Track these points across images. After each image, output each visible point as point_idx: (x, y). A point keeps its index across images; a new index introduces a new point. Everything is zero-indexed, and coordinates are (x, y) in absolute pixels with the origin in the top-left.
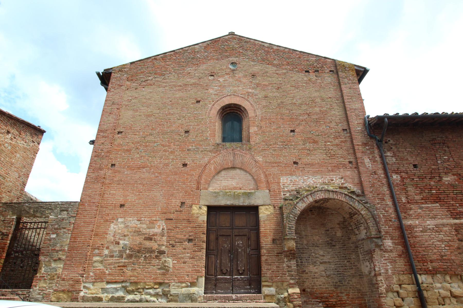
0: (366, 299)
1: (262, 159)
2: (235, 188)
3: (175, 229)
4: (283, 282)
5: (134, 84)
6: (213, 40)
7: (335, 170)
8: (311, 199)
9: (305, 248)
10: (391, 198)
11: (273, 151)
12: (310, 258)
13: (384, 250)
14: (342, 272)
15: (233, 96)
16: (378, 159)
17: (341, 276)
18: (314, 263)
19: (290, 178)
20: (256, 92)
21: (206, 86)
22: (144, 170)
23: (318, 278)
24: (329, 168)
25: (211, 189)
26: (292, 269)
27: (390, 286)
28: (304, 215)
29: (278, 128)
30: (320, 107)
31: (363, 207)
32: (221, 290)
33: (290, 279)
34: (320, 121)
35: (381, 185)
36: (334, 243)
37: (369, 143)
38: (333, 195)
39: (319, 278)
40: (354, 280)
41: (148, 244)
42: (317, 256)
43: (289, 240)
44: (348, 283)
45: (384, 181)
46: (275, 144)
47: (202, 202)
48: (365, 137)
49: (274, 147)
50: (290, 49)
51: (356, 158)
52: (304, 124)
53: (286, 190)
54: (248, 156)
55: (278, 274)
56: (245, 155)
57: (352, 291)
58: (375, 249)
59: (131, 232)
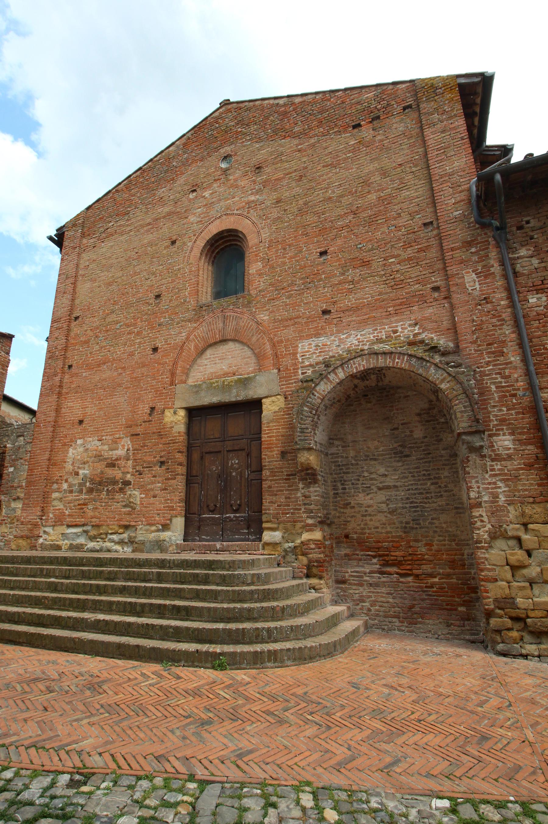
0: (466, 552)
1: (267, 317)
2: (226, 374)
3: (142, 449)
4: (295, 522)
5: (92, 241)
6: (195, 127)
7: (403, 310)
8: (341, 375)
9: (352, 464)
10: (520, 348)
11: (286, 298)
12: (359, 480)
13: (493, 456)
14: (421, 502)
15: (224, 217)
16: (496, 268)
17: (418, 511)
18: (367, 490)
19: (314, 342)
20: (264, 197)
21: (185, 211)
22: (105, 367)
23: (373, 516)
24: (389, 309)
25: (190, 382)
26: (311, 501)
27: (501, 526)
28: (352, 405)
29: (297, 254)
30: (379, 190)
31: (445, 374)
32: (207, 536)
33: (308, 517)
34: (378, 218)
35: (498, 323)
36: (406, 451)
37: (479, 239)
38: (386, 360)
39: (375, 515)
40: (443, 517)
41: (111, 473)
42: (373, 476)
43: (300, 451)
44: (430, 523)
45: (507, 314)
46: (292, 284)
47: (178, 404)
48: (469, 227)
49: (289, 291)
50: (324, 92)
51: (447, 278)
52: (346, 234)
53: (307, 363)
54: (246, 316)
55: (288, 509)
56: (241, 316)
57: (437, 538)
58: (469, 457)
59: (91, 457)
